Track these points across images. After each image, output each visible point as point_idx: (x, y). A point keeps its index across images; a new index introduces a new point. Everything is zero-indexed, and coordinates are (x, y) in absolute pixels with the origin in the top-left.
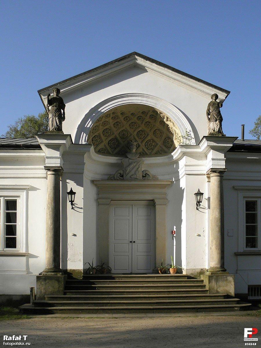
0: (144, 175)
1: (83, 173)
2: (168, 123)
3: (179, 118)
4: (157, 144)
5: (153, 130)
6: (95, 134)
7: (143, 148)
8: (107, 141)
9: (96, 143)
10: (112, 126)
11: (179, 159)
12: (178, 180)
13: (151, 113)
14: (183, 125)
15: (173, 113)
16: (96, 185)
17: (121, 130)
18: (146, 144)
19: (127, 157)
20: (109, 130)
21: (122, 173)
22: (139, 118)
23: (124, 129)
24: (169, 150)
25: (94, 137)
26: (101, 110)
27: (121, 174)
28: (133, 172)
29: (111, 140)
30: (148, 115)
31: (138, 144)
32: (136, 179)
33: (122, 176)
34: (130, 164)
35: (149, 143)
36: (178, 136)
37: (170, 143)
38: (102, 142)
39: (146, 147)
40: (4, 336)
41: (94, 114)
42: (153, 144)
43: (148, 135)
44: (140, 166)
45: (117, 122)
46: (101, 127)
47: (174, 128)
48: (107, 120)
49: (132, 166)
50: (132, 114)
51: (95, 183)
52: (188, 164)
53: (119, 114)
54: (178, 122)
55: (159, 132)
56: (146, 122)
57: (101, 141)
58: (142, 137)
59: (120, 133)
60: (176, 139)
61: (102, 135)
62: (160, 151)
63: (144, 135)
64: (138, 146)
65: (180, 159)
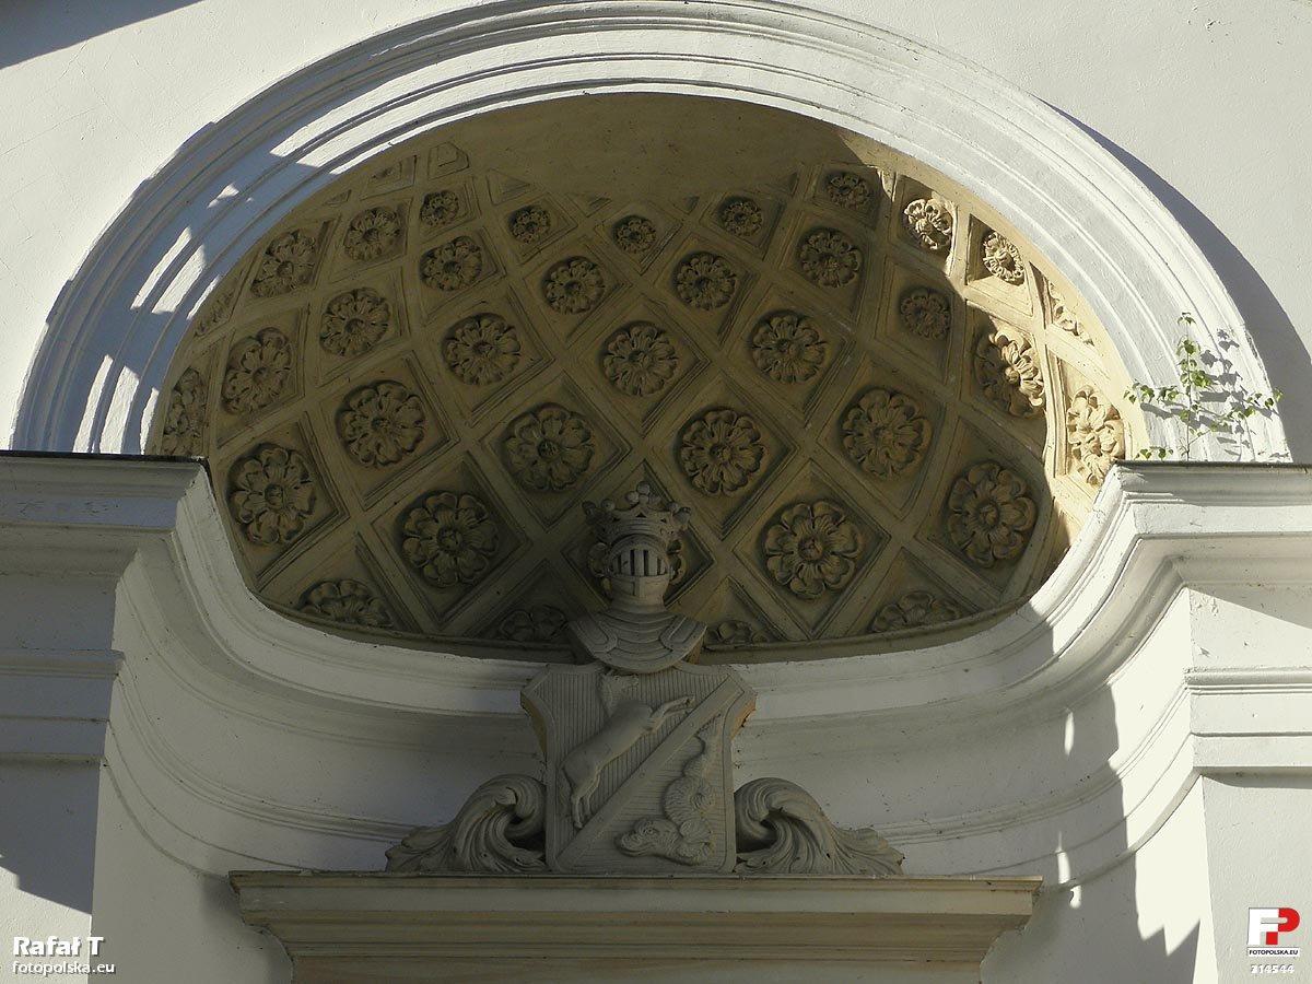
0: (759, 832)
1: (91, 763)
2: (987, 294)
3: (1097, 223)
4: (881, 538)
5: (835, 400)
6: (262, 428)
7: (745, 577)
8: (388, 509)
9: (269, 519)
10: (433, 362)
11: (1115, 641)
12: (1108, 870)
13: (809, 209)
14: (1148, 285)
15: (1039, 173)
16: (262, 926)
17: (522, 400)
18: (770, 543)
19: (580, 656)
20: (405, 397)
21: (529, 805)
22: (693, 276)
23: (547, 394)
24: (1002, 589)
25: (254, 454)
26: (301, 152)
27: (516, 820)
28: (639, 798)
29: (420, 503)
30: (786, 238)
31: (688, 535)
32: (674, 867)
33: (535, 841)
34: (610, 722)
35: (802, 530)
36: (1098, 418)
37: (1010, 515)
38: (337, 513)
39: (769, 575)
40: (17, 940)
41: (230, 191)
42: (842, 539)
43: (785, 452)
44: (713, 742)
45: (478, 318)
46: (315, 358)
47: (1051, 339)
48: (375, 278)
49: (627, 740)
50: (627, 231)
51: (253, 898)
52: (1226, 661)
53: (495, 226)
54: (1086, 258)
55: (899, 417)
56: (767, 320)
57: (321, 509)
58: (731, 476)
59: (508, 435)
60: (1073, 453)
61: (330, 450)
62: (907, 604)
63: (747, 459)
64: (692, 565)
65: (1127, 641)
